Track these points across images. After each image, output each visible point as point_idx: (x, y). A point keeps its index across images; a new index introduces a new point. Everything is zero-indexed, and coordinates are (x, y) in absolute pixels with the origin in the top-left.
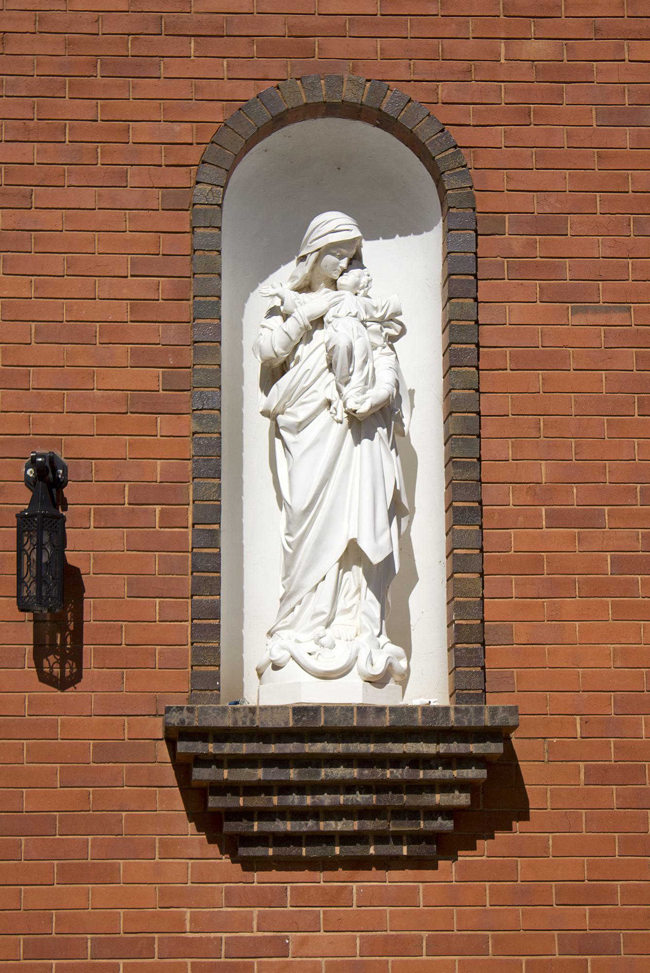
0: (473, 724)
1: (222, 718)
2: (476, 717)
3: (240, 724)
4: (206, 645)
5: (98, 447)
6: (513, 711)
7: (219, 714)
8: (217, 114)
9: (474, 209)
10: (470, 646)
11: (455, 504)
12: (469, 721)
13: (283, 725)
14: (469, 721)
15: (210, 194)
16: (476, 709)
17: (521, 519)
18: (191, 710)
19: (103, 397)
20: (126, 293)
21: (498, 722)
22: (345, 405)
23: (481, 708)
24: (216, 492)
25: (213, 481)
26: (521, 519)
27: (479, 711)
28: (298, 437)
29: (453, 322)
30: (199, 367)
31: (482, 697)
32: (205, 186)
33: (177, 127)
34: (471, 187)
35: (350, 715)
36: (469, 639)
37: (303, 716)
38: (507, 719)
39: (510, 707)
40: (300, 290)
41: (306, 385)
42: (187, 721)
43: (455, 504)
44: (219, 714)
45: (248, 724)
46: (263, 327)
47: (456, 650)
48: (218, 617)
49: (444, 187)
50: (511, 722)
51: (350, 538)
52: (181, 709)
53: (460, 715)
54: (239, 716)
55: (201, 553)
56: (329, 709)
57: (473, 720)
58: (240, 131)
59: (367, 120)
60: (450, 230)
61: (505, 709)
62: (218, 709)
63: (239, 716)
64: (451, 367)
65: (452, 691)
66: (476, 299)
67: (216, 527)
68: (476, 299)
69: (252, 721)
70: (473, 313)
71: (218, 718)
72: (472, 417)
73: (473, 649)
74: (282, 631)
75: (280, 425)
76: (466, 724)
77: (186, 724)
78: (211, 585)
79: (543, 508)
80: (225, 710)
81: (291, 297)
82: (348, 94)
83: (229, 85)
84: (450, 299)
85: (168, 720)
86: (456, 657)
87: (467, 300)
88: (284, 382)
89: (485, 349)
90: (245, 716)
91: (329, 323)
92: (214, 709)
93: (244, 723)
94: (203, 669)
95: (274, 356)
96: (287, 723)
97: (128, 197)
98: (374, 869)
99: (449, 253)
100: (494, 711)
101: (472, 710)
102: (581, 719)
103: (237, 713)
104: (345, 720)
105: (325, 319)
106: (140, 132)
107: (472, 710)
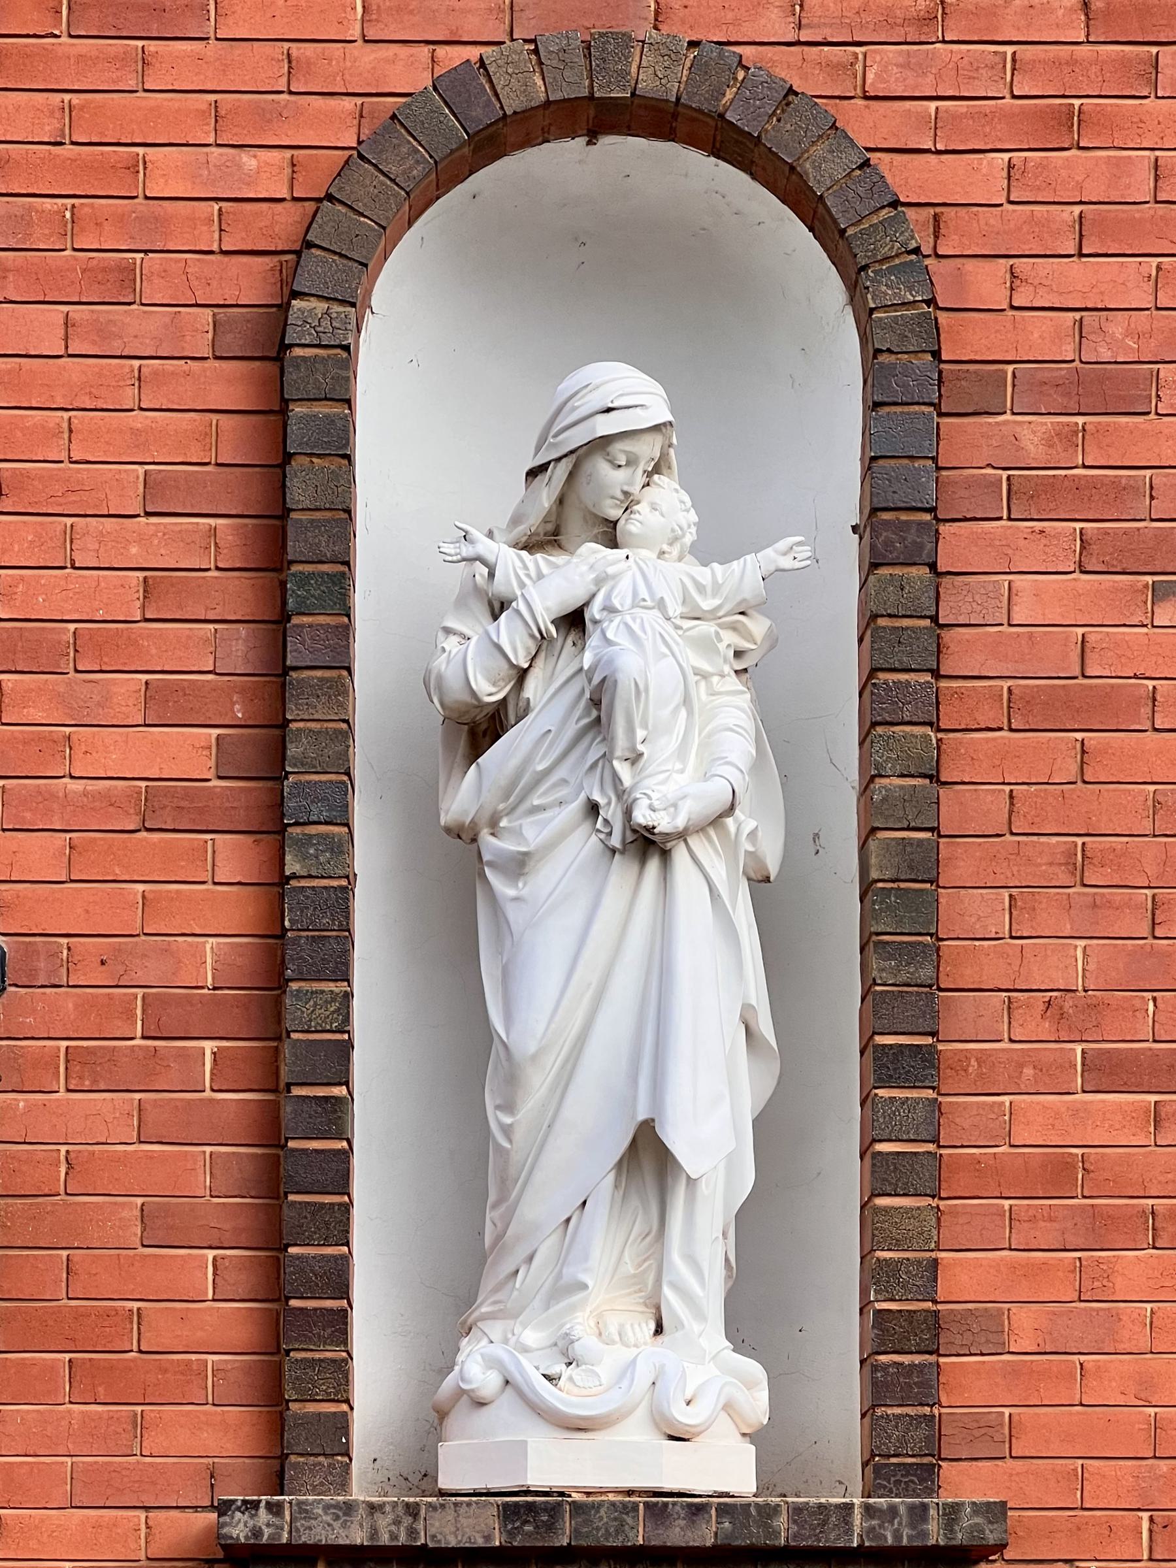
0: (905, 1542)
1: (344, 1525)
2: (912, 1526)
3: (385, 1539)
4: (317, 1356)
5: (72, 909)
6: (997, 1511)
7: (337, 1518)
8: (336, 127)
9: (936, 354)
10: (906, 1359)
11: (879, 1040)
12: (897, 1535)
13: (480, 1542)
14: (897, 1535)
15: (326, 323)
16: (911, 1508)
17: (1028, 1071)
18: (275, 1509)
19: (85, 794)
20: (135, 554)
21: (960, 1538)
22: (628, 813)
23: (925, 1507)
24: (338, 1010)
25: (331, 986)
26: (1028, 1071)
27: (919, 1514)
28: (523, 888)
29: (882, 622)
30: (301, 725)
31: (926, 1476)
32: (313, 303)
33: (249, 161)
34: (928, 302)
35: (629, 1520)
36: (907, 1341)
37: (526, 1522)
38: (983, 1531)
39: (989, 1503)
40: (530, 546)
41: (540, 768)
42: (267, 1532)
43: (879, 1040)
44: (337, 1518)
45: (403, 1539)
46: (448, 631)
47: (875, 1368)
48: (343, 1290)
49: (866, 301)
50: (991, 1538)
51: (641, 1117)
52: (255, 1505)
53: (874, 1522)
54: (383, 1523)
55: (305, 1151)
56: (585, 1508)
57: (906, 1532)
58: (393, 169)
59: (692, 141)
60: (877, 405)
61: (977, 1508)
62: (337, 1506)
63: (383, 1523)
64: (874, 724)
65: (867, 1456)
66: (933, 566)
67: (340, 1091)
68: (933, 566)
69: (412, 1532)
70: (927, 601)
71: (337, 1525)
72: (920, 842)
73: (912, 1366)
74: (489, 1322)
75: (486, 857)
76: (890, 1541)
77: (264, 1540)
78: (327, 1224)
79: (1079, 1048)
80: (349, 1508)
81: (512, 564)
82: (650, 77)
83: (370, 56)
84: (874, 566)
85: (225, 1531)
86: (875, 1383)
87: (914, 571)
88: (501, 755)
89: (955, 684)
90: (397, 1522)
91: (596, 622)
92: (327, 1507)
93: (394, 1537)
94: (311, 1408)
95: (61, 794)
96: (488, 1538)
97: (139, 327)
98: (833, 1563)
99: (873, 459)
100: (952, 1512)
101: (902, 1510)
102: (1151, 1519)
103: (377, 1515)
104: (617, 1532)
105: (587, 616)
106: (168, 172)
107: (902, 1510)
